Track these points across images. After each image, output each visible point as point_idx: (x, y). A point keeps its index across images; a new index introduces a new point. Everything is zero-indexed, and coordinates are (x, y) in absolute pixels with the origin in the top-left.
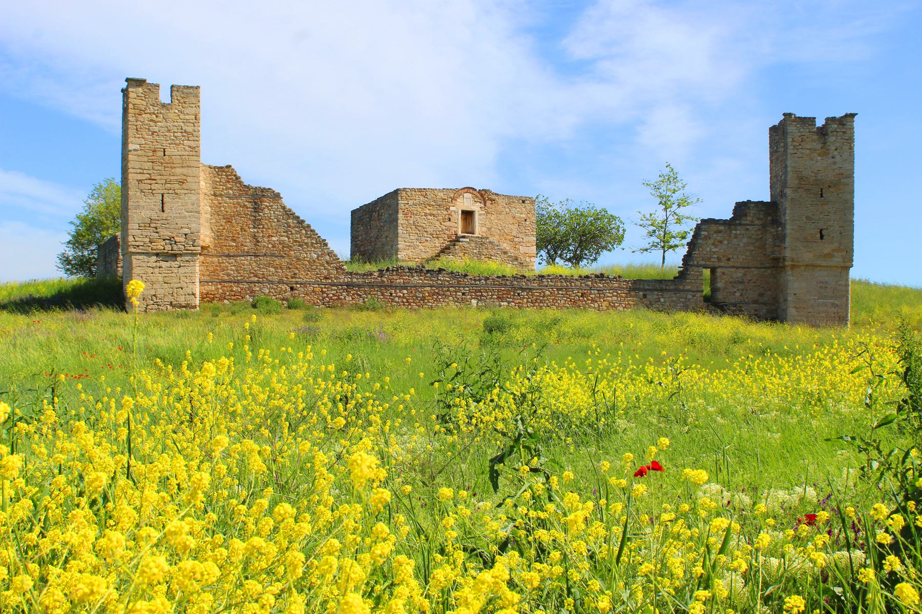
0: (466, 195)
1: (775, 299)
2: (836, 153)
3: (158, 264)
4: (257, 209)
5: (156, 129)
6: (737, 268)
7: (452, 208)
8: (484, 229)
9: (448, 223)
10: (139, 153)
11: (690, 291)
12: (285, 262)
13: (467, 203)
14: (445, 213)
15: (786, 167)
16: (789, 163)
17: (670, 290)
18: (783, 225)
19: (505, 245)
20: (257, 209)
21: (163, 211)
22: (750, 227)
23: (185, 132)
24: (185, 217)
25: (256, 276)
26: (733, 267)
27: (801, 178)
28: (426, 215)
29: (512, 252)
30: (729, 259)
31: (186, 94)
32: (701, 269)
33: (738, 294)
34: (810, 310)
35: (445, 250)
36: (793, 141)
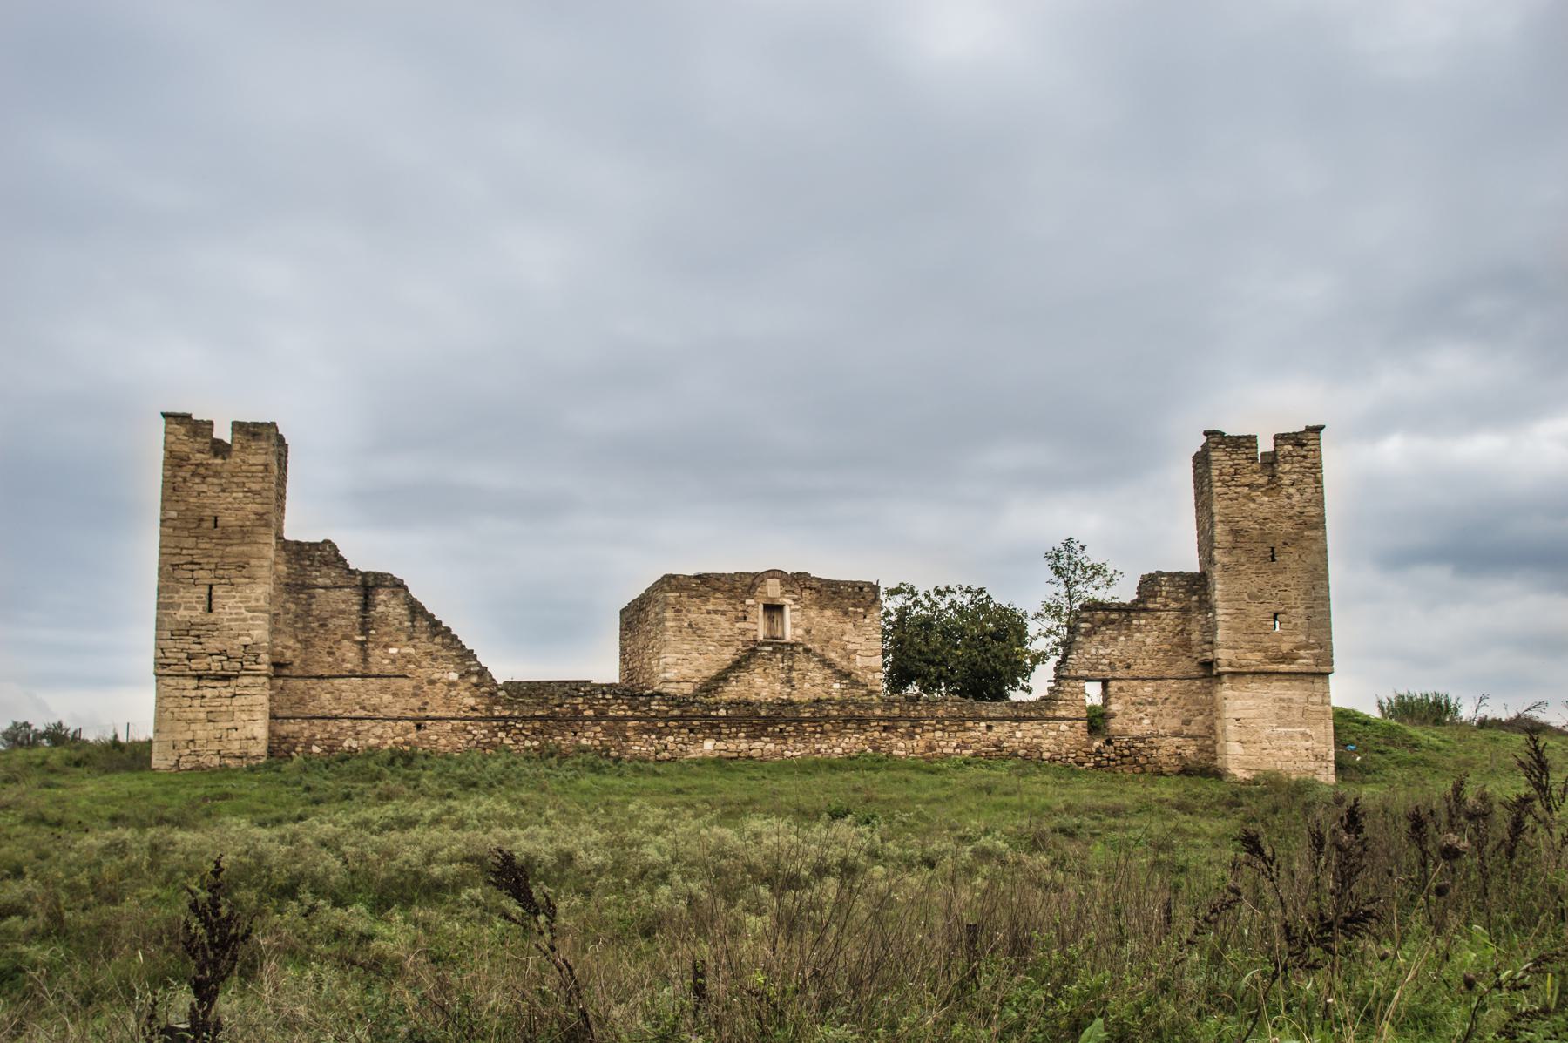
0: (770, 581)
1: (1211, 728)
2: (1292, 490)
3: (200, 693)
4: (367, 605)
5: (204, 488)
6: (1144, 680)
8: (800, 632)
9: (741, 625)
10: (178, 523)
11: (1064, 718)
12: (406, 684)
13: (773, 589)
15: (1212, 515)
16: (1215, 509)
17: (1031, 719)
18: (1212, 608)
19: (832, 655)
20: (367, 605)
21: (210, 610)
22: (1164, 614)
24: (244, 620)
25: (363, 708)
26: (1137, 678)
27: (1236, 533)
28: (709, 612)
29: (843, 664)
30: (1128, 667)
31: (211, 423)
32: (1081, 683)
33: (1146, 721)
34: (1266, 744)
35: (738, 665)
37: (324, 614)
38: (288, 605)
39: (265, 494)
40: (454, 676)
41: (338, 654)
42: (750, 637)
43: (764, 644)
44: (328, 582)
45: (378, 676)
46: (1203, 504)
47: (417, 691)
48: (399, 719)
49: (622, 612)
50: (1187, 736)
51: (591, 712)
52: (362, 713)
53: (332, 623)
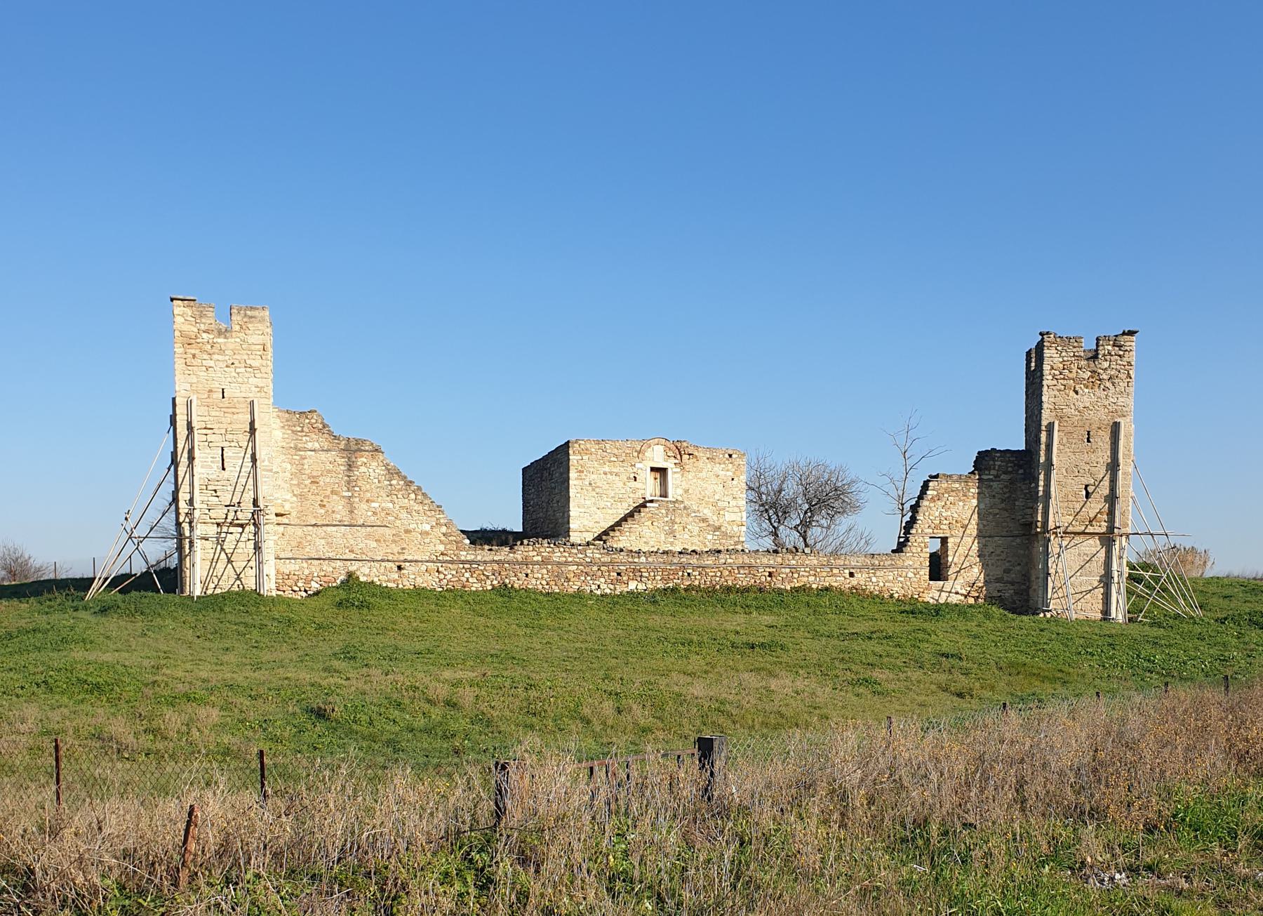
1: (1026, 577)
5: (211, 363)
7: (638, 465)
8: (680, 491)
9: (633, 484)
14: (630, 469)
17: (884, 567)
19: (706, 511)
23: (251, 367)
28: (605, 474)
29: (713, 519)
36: (1052, 368)
37: (315, 474)
38: (284, 465)
39: (263, 370)
40: (427, 528)
41: (329, 507)
42: (639, 494)
43: (651, 501)
44: (317, 446)
45: (363, 525)
46: (1033, 393)
47: (396, 539)
48: (383, 561)
49: (524, 469)
50: (1008, 582)
51: (539, 558)
52: (352, 556)
53: (322, 481)
